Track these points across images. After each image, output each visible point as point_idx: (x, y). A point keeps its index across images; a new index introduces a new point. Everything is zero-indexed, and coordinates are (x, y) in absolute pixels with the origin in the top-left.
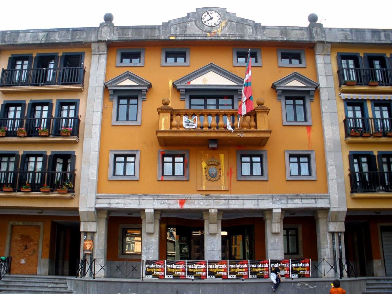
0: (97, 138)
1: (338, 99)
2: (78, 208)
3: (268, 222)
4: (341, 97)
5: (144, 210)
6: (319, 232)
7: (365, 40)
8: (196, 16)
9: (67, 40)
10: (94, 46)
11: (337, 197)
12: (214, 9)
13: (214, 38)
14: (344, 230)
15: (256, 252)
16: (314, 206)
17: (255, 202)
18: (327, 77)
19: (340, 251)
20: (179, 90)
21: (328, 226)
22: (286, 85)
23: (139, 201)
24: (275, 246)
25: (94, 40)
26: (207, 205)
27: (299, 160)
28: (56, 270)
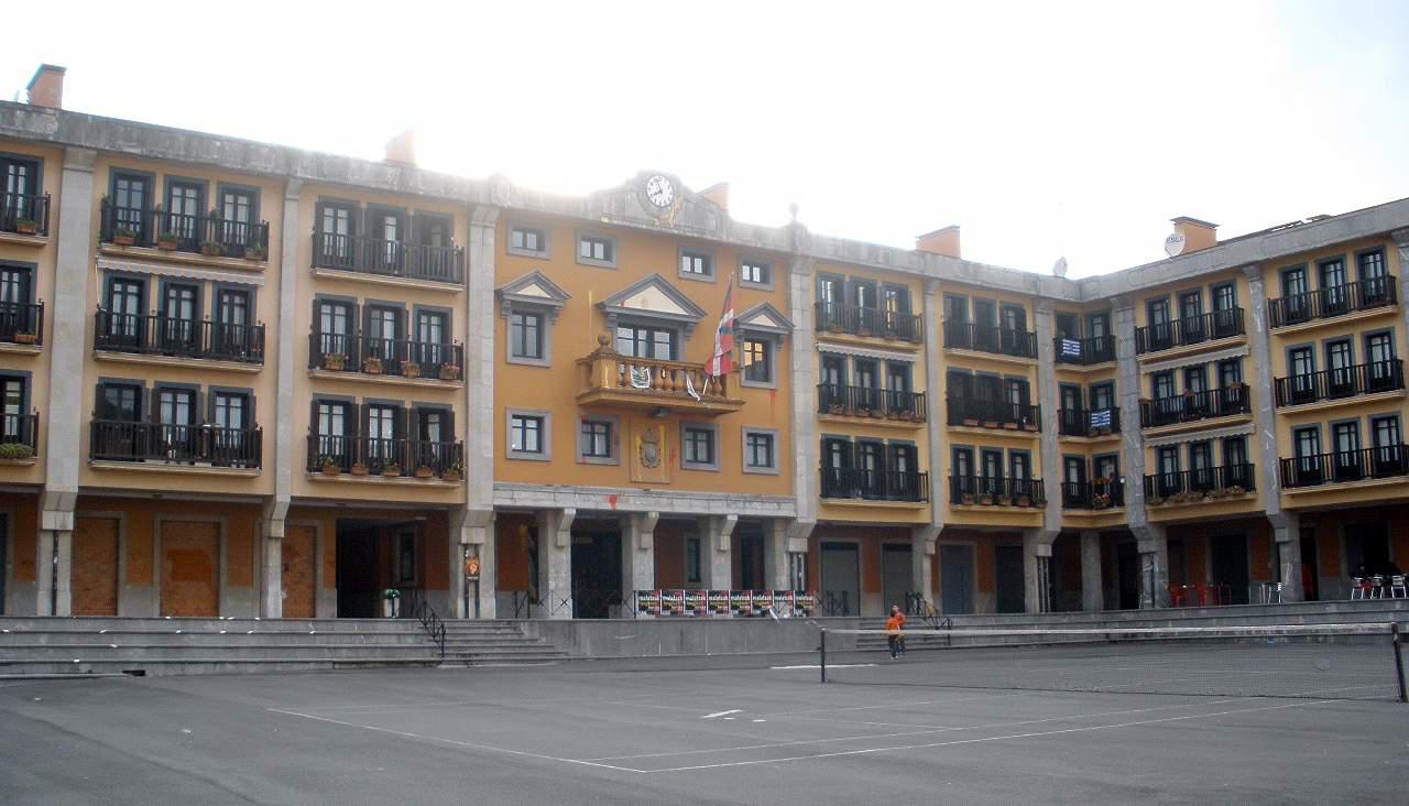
1: (812, 349)
8: (640, 186)
13: (663, 230)
15: (695, 579)
17: (705, 503)
19: (799, 579)
21: (786, 543)
22: (519, 293)
24: (721, 571)
26: (645, 505)
27: (524, 424)
28: (346, 610)
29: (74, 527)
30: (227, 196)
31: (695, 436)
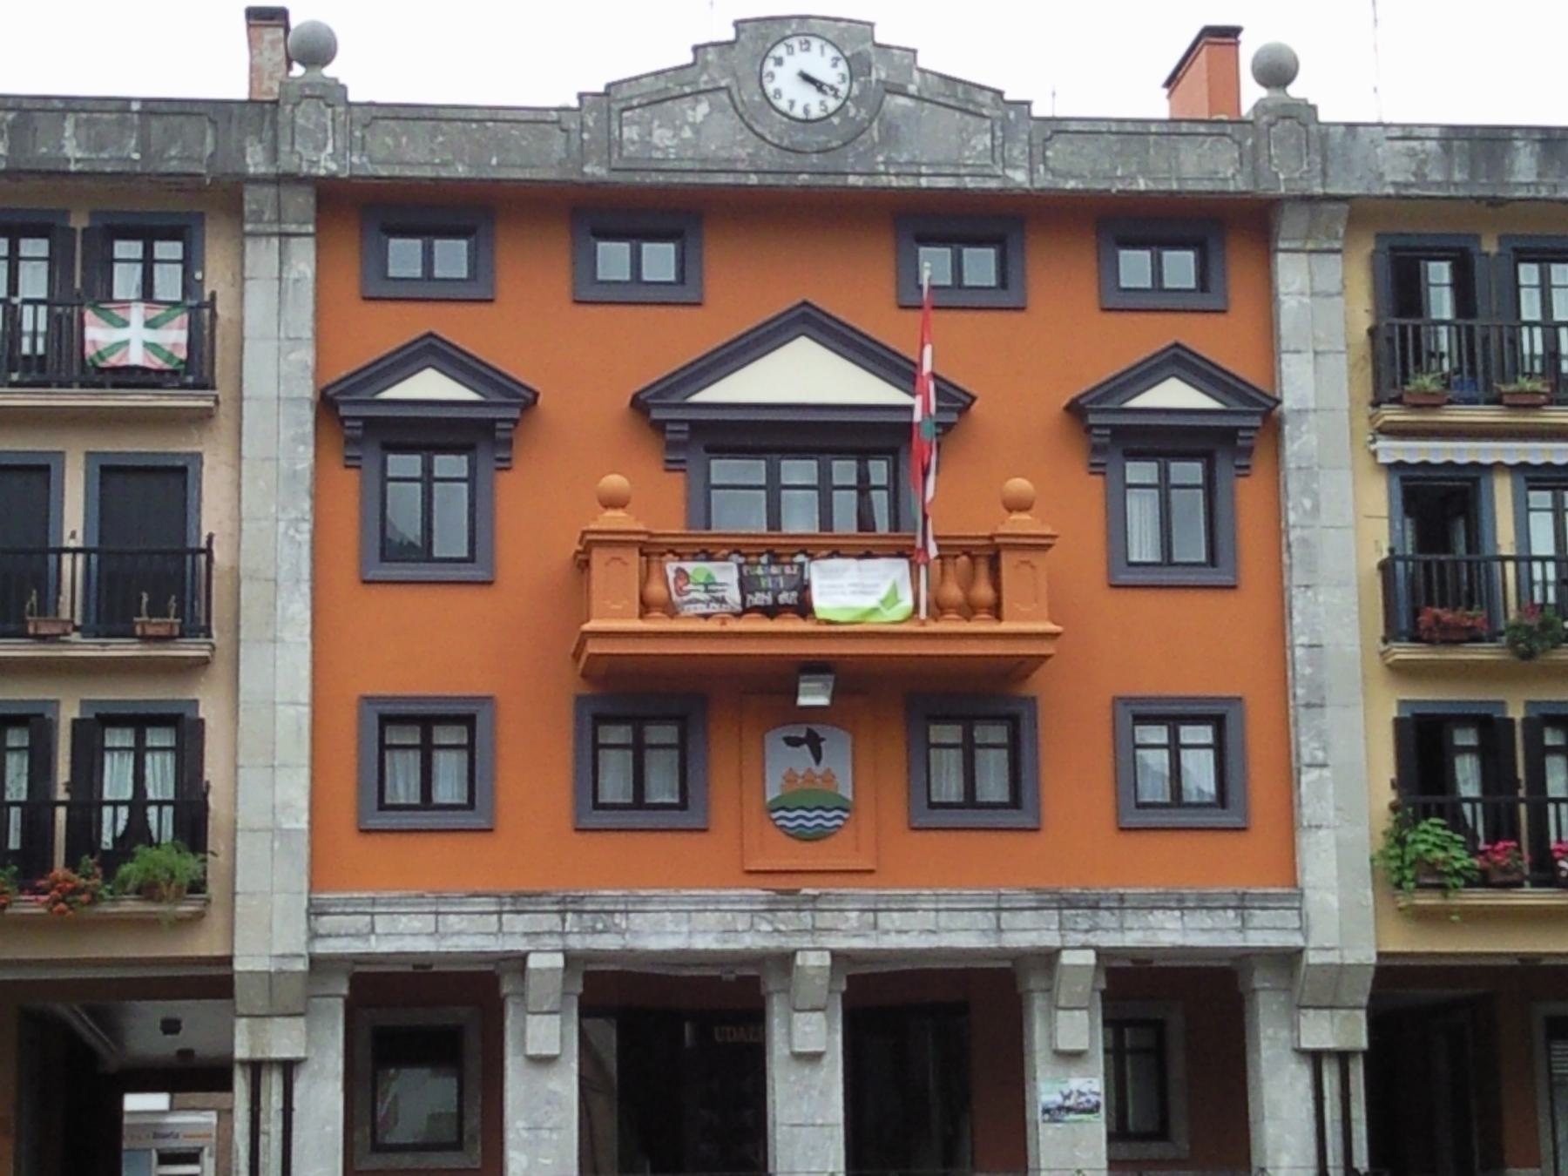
0: (304, 644)
1: (1366, 462)
2: (228, 960)
3: (1038, 1003)
4: (1374, 454)
5: (522, 958)
6: (1258, 1050)
7: (1508, 184)
9: (120, 159)
10: (252, 198)
11: (1336, 905)
12: (817, 26)
14: (1363, 1042)
16: (1234, 940)
17: (986, 920)
18: (1320, 359)
20: (659, 427)
21: (1295, 1027)
23: (500, 920)
25: (262, 170)
29: (1371, 1041)
30: (1522, 268)
31: (140, 738)
